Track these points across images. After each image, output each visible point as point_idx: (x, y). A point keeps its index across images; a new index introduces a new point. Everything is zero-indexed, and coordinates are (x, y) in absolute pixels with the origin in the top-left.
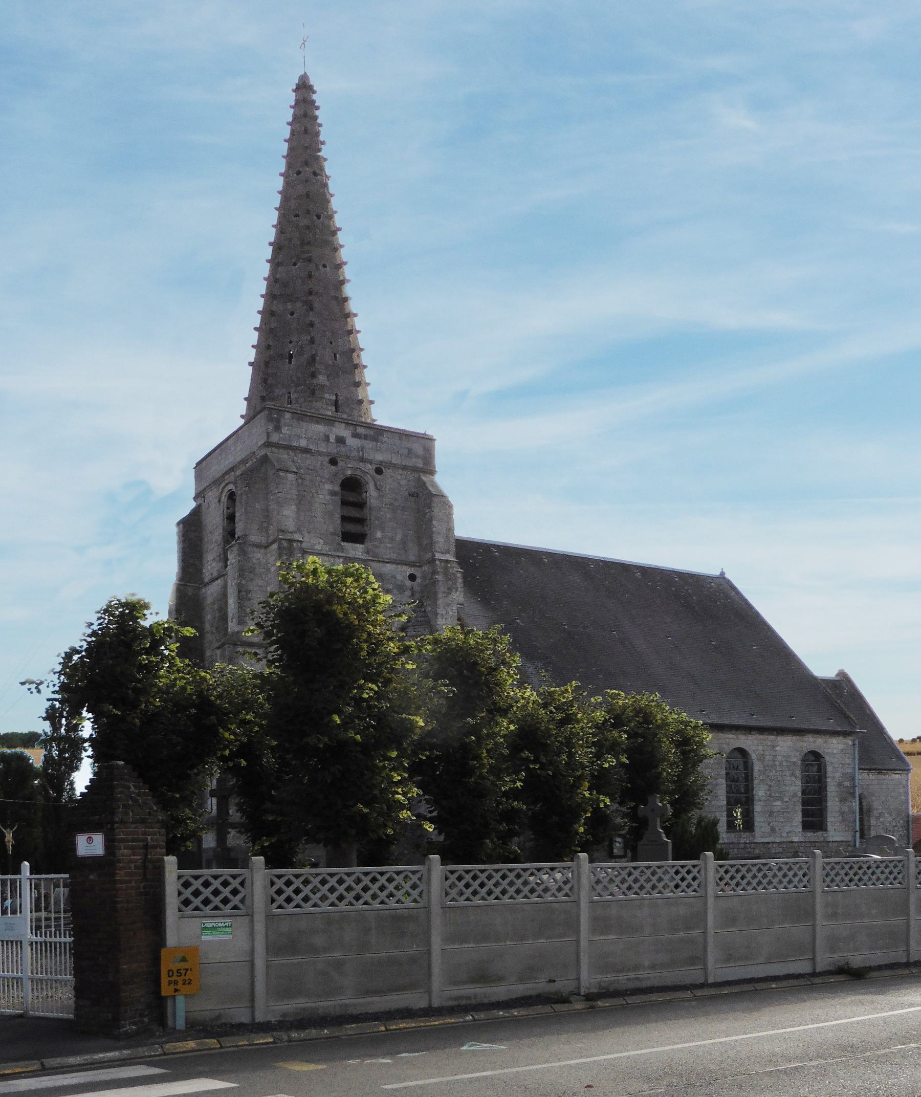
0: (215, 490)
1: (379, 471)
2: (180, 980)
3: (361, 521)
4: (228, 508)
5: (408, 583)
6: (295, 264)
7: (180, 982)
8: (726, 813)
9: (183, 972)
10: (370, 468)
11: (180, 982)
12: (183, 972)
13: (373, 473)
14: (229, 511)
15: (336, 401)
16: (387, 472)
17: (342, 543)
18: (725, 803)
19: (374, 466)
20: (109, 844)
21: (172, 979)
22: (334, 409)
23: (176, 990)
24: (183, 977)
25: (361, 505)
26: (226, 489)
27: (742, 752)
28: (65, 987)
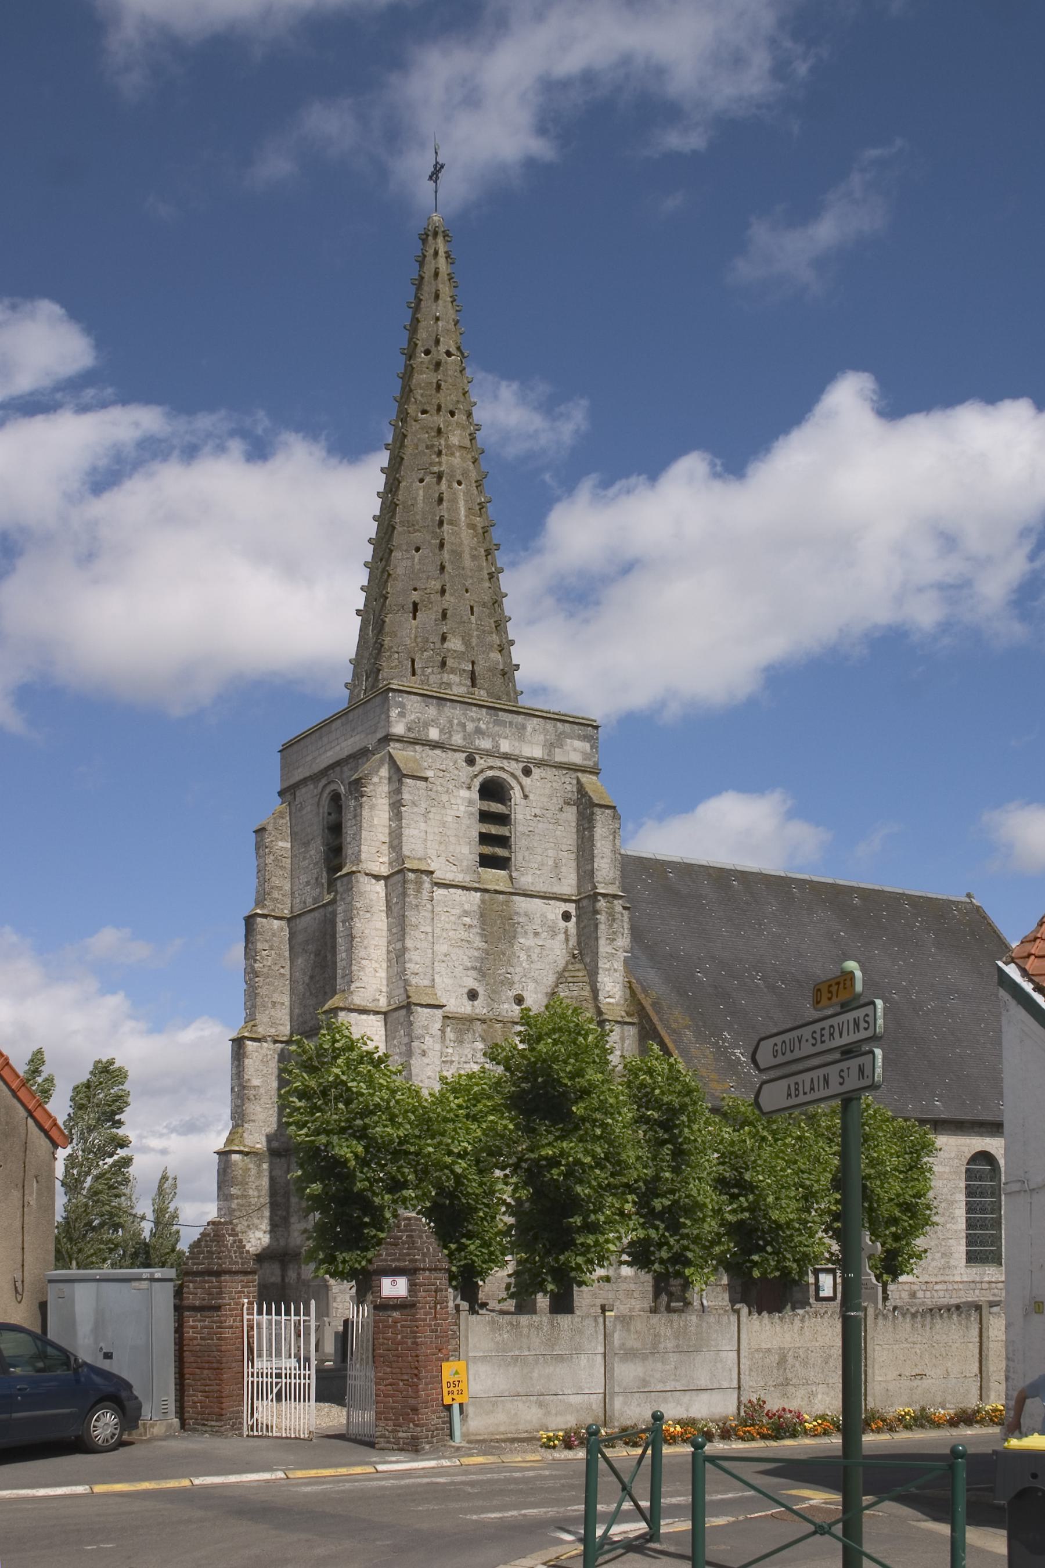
0: (312, 787)
1: (527, 772)
2: (455, 1390)
3: (503, 841)
4: (329, 814)
5: (562, 924)
6: (421, 481)
7: (456, 1392)
8: (965, 1240)
9: (457, 1383)
10: (516, 767)
11: (456, 1392)
12: (457, 1383)
13: (519, 773)
14: (330, 817)
15: (473, 672)
16: (536, 772)
17: (480, 869)
18: (964, 1227)
19: (521, 765)
20: (412, 1286)
21: (450, 1389)
22: (469, 683)
23: (453, 1399)
24: (457, 1388)
25: (503, 819)
26: (327, 791)
27: (984, 1157)
28: (882, 1163)
